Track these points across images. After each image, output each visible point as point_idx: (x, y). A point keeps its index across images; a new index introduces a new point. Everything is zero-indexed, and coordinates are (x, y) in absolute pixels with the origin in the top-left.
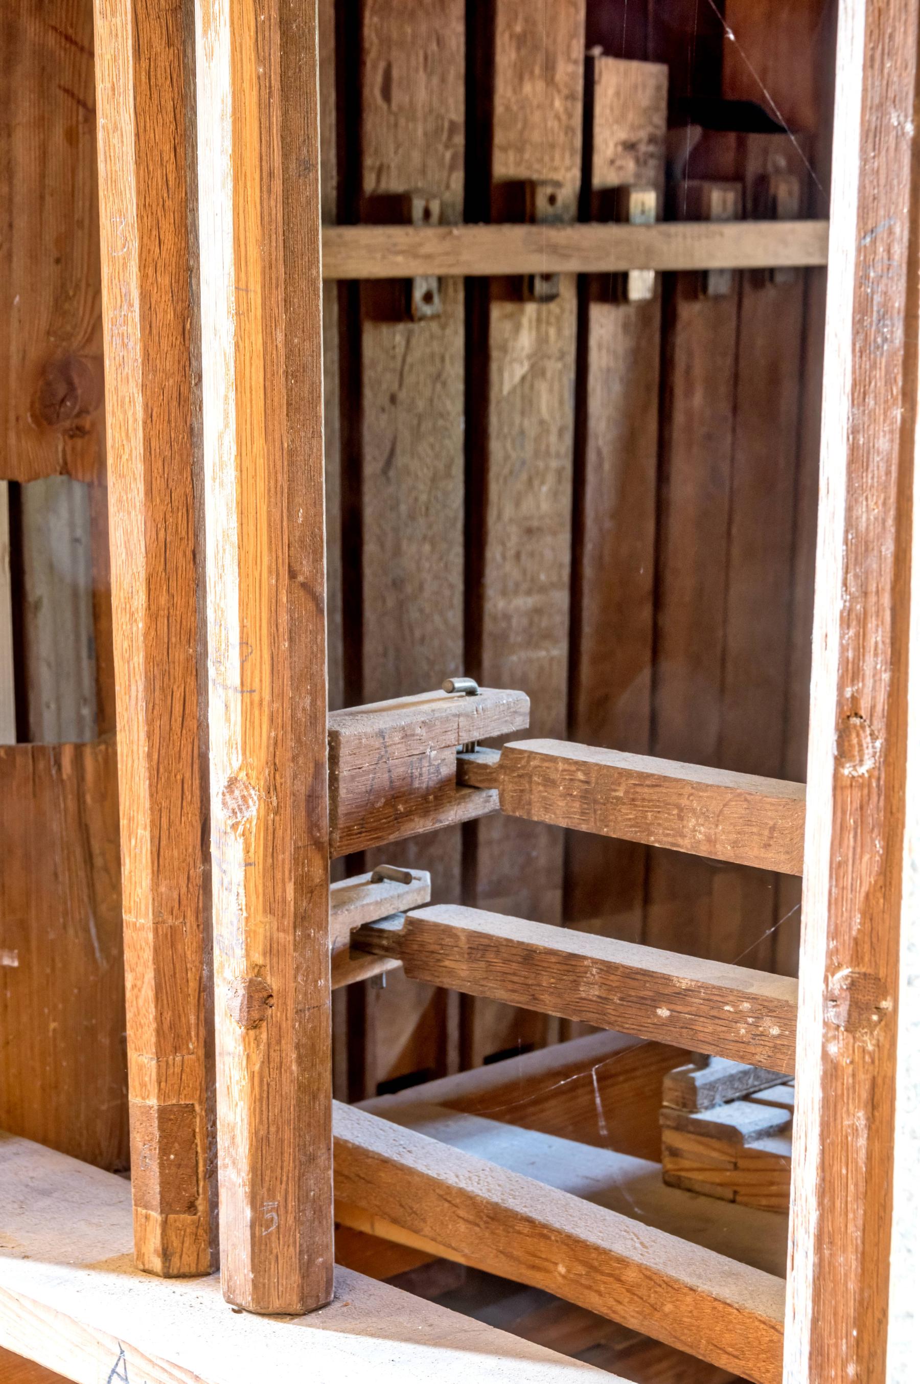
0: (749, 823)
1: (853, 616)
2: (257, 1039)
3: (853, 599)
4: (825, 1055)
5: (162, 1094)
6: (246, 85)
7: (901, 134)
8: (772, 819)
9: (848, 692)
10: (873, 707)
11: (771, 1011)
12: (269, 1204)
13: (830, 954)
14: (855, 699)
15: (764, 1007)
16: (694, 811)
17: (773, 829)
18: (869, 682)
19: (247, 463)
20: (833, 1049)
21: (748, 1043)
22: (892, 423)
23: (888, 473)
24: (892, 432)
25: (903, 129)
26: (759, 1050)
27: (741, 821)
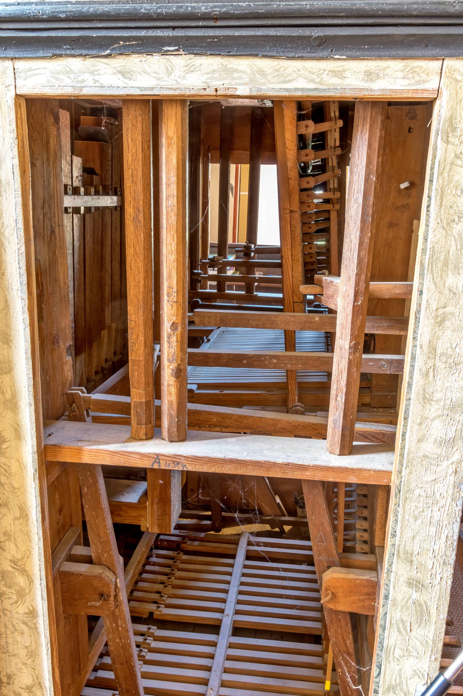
0: (267, 320)
2: (178, 380)
3: (359, 270)
4: (349, 358)
5: (146, 398)
6: (180, 161)
7: (373, 180)
9: (357, 289)
12: (181, 417)
13: (351, 339)
14: (358, 290)
16: (252, 320)
17: (274, 321)
19: (179, 249)
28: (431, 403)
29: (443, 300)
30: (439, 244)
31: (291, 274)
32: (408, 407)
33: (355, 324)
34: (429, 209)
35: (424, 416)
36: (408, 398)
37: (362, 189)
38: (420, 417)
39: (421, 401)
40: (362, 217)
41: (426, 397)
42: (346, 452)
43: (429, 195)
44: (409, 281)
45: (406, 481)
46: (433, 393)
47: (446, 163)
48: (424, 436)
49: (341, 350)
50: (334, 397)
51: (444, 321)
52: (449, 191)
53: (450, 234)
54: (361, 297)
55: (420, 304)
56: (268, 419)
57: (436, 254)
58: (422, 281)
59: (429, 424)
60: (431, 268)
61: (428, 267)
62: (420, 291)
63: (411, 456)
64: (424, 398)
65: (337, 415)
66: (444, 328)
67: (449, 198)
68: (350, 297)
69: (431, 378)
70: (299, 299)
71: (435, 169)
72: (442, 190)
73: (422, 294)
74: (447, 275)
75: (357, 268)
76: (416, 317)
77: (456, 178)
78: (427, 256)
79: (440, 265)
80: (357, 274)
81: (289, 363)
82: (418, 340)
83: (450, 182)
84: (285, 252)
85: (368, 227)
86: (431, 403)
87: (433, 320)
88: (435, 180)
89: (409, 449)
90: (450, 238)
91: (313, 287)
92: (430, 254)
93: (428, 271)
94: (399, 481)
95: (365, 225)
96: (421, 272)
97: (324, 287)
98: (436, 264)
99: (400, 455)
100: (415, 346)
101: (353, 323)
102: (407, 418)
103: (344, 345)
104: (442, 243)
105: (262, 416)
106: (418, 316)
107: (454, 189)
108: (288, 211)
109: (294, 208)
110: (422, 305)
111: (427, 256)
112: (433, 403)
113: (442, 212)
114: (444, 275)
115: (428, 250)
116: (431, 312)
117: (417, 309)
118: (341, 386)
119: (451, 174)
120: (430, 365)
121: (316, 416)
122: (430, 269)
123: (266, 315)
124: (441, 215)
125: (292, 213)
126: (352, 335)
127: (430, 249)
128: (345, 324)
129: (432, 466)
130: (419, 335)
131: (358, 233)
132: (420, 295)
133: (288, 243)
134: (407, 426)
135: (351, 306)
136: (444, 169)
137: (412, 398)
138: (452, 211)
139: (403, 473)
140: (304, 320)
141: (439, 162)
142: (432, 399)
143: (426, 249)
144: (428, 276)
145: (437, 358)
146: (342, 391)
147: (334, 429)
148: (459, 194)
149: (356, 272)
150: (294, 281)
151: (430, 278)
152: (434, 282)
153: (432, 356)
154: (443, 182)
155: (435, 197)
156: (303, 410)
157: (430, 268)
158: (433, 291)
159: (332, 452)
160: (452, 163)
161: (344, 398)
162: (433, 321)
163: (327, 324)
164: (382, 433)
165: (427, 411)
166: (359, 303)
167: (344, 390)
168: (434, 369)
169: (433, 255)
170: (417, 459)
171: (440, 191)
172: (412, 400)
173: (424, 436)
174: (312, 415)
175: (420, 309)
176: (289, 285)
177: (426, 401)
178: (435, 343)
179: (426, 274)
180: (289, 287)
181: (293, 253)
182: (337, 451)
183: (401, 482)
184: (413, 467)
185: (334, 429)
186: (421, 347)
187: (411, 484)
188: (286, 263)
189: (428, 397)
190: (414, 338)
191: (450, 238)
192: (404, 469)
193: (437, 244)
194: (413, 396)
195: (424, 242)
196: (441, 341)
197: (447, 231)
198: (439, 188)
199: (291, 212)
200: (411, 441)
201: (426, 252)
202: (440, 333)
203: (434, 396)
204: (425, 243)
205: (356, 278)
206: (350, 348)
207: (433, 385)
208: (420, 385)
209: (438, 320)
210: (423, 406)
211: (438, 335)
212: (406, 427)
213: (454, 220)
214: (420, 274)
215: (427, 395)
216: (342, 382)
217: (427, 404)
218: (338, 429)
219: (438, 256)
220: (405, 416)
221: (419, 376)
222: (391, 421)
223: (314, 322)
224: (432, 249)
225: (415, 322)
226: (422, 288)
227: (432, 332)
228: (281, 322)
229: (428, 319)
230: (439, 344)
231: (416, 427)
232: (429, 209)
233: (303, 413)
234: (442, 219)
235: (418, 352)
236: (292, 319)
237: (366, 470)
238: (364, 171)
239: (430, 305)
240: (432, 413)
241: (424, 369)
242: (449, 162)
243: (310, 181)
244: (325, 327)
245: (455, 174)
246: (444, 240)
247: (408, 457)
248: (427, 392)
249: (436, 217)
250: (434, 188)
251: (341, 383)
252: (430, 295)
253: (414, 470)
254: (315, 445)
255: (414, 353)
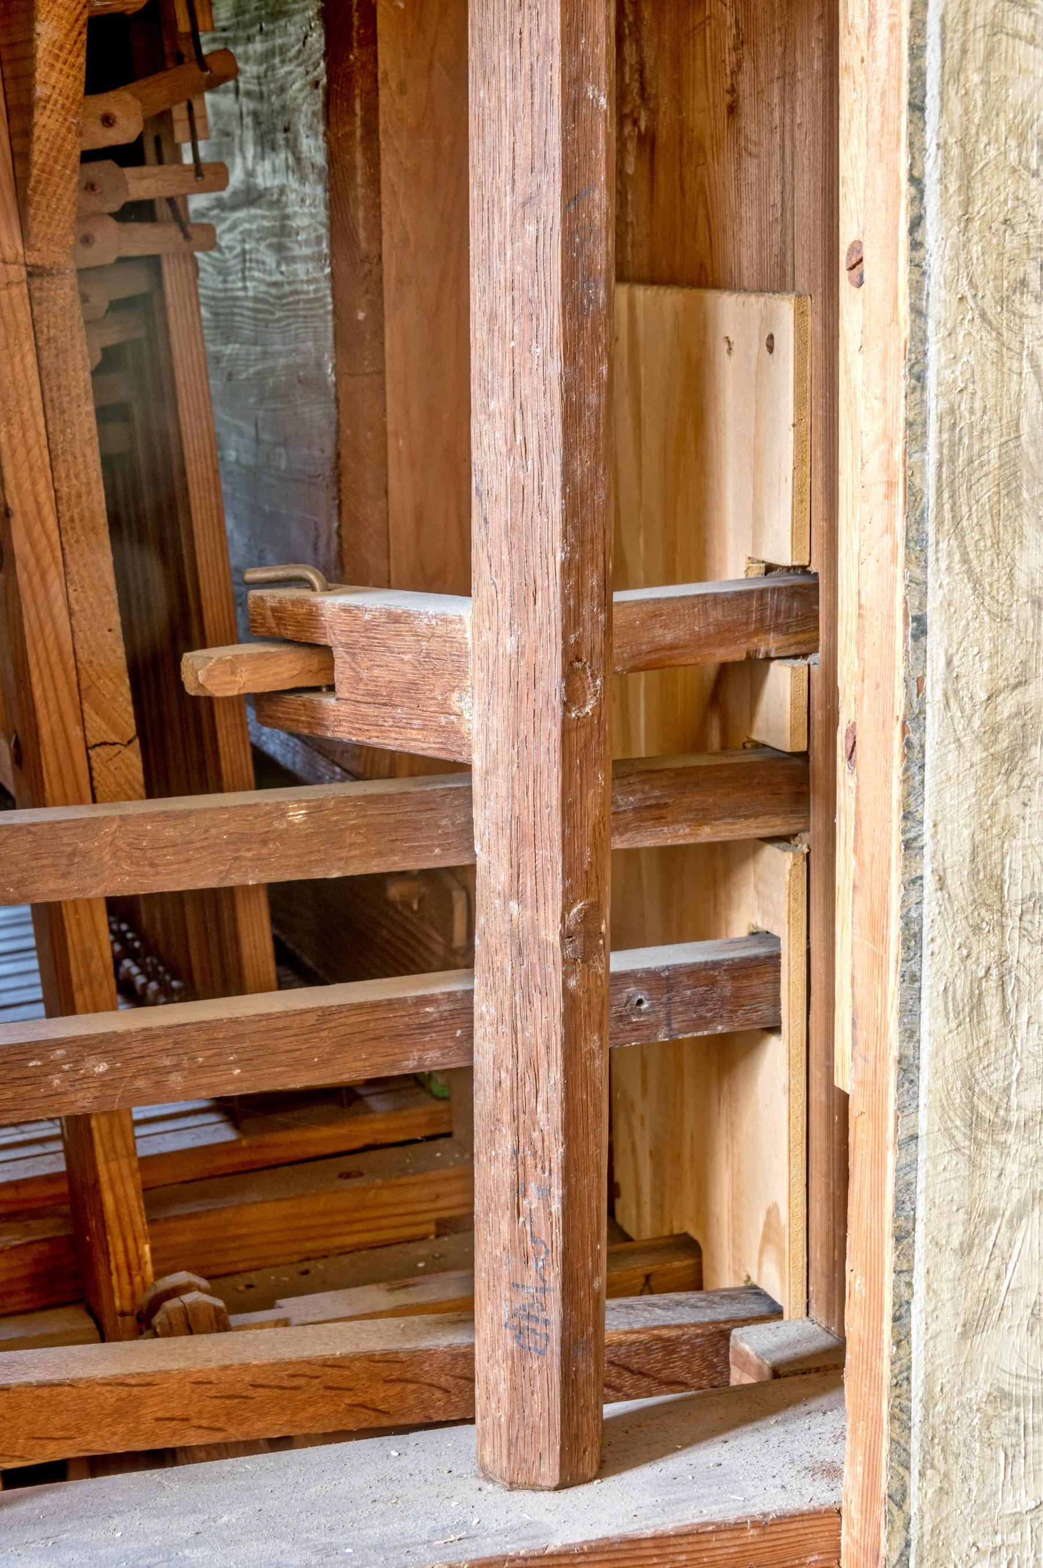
0: (36, 857)
1: (573, 566)
3: (573, 548)
4: (566, 992)
7: (595, 108)
8: (68, 845)
10: (593, 649)
11: (93, 1049)
13: (565, 894)
14: (577, 643)
15: (84, 1046)
18: (588, 625)
20: (572, 983)
21: (65, 1093)
22: (599, 379)
23: (597, 426)
24: (599, 387)
25: (598, 101)
26: (80, 1095)
27: (26, 856)
28: (1002, 1138)
29: (1014, 651)
30: (973, 394)
31: (60, 601)
32: (910, 1177)
33: (578, 817)
34: (918, 236)
35: (980, 1205)
36: (903, 1135)
37: (556, 153)
38: (962, 1216)
39: (959, 1137)
40: (566, 288)
41: (979, 1117)
42: (589, 1463)
43: (916, 174)
44: (636, 586)
45: (927, 1538)
46: (1007, 1089)
47: (971, 27)
48: (987, 1301)
49: (520, 953)
50: (506, 1195)
51: (1025, 749)
52: (992, 152)
53: (1015, 345)
54: (594, 679)
55: (920, 682)
56: (91, 1383)
57: (966, 441)
58: (917, 573)
59: (1003, 1242)
60: (952, 510)
61: (940, 505)
62: (916, 619)
63: (939, 1408)
64: (975, 1120)
65: (531, 1279)
66: (1027, 782)
67: (995, 183)
68: (542, 685)
69: (994, 1022)
70: (114, 728)
71: (929, 49)
72: (963, 146)
73: (924, 632)
74: (1018, 534)
75: (565, 536)
76: (908, 744)
77: (1016, 94)
78: (932, 456)
79: (986, 490)
80: (568, 568)
81: (177, 1067)
82: (927, 851)
83: (992, 111)
84: (18, 487)
85: (594, 330)
86: (1002, 1138)
87: (979, 748)
88: (932, 104)
89: (929, 1377)
90: (1015, 365)
91: (261, 656)
92: (941, 445)
93: (940, 522)
94: (898, 1542)
95: (581, 327)
96: (913, 533)
97: (339, 653)
98: (969, 489)
99: (893, 1417)
100: (913, 882)
101: (568, 809)
102: (908, 1233)
103: (535, 928)
104: (985, 390)
105: (56, 1377)
106: (914, 738)
107: (1013, 143)
108: (18, 273)
109: (46, 255)
110: (928, 683)
111: (932, 456)
112: (1010, 1137)
113: (976, 249)
114: (1007, 537)
115: (933, 426)
116: (968, 712)
117: (909, 705)
118: (536, 1135)
119: (994, 77)
120: (984, 963)
121: (286, 1323)
122: (948, 516)
123: (28, 829)
124: (968, 264)
125: (37, 282)
126: (568, 872)
127: (940, 419)
128: (528, 818)
129: (1030, 1439)
130: (927, 827)
131: (555, 367)
132: (916, 637)
133: (31, 436)
134: (910, 1271)
135: (552, 729)
136: (964, 52)
137: (922, 1131)
138: (1012, 243)
139: (913, 1505)
140: (232, 827)
141: (943, 20)
142: (1005, 1122)
143: (924, 423)
144: (943, 545)
145: (1012, 923)
146: (542, 1160)
147: (522, 1358)
148: (1034, 165)
149: (559, 556)
150: (80, 635)
151: (950, 555)
152: (970, 572)
153: (987, 916)
154: (966, 112)
155: (940, 180)
156: (220, 1303)
157: (947, 507)
158: (969, 614)
159: (521, 1479)
160: (993, 25)
161: (557, 1192)
162: (978, 754)
163: (351, 838)
164: (659, 1339)
165: (991, 1182)
166: (588, 709)
167: (557, 1153)
168: (1002, 977)
169: (952, 445)
170: (965, 1421)
171: (955, 151)
172: (922, 1141)
173: (987, 1301)
174: (262, 1326)
175: (922, 702)
176: (54, 657)
177: (981, 1136)
178: (996, 857)
179: (932, 539)
180: (58, 671)
181: (64, 490)
182: (549, 1469)
183: (908, 1545)
184: (951, 1459)
185: (522, 1358)
186: (942, 884)
187: (946, 1543)
188: (33, 545)
189: (988, 1114)
190: (907, 845)
191: (1015, 365)
192: (914, 1482)
193: (966, 396)
194: (924, 1121)
195: (914, 390)
196: (1019, 843)
197: (1000, 334)
198: (951, 140)
199: (30, 274)
200: (934, 1337)
201: (924, 434)
202: (1015, 804)
203: (1014, 1101)
204: (917, 395)
205: (563, 588)
206: (566, 936)
207: (1003, 1052)
208: (949, 1063)
209: (998, 747)
210: (972, 1162)
211: (1007, 816)
212: (905, 1278)
213: (1024, 283)
214: (908, 541)
215: (982, 1107)
216: (542, 1117)
217: (989, 1149)
218: (542, 1353)
219: (976, 448)
220: (901, 1222)
221: (941, 1021)
222: (648, 1277)
223: (282, 836)
224: (947, 421)
225: (906, 769)
226: (922, 605)
227: (979, 802)
228: (114, 855)
229: (960, 746)
230: (1015, 859)
231: (950, 1267)
232: (918, 236)
233: (219, 1324)
234: (980, 282)
235: (930, 910)
236: (169, 832)
237: (721, 1528)
238: (557, 64)
239: (963, 680)
240: (1011, 1188)
241: (961, 986)
242: (980, 20)
243: (116, 111)
244: (344, 853)
245: (1011, 74)
246: (991, 375)
247: (926, 1418)
248: (983, 1092)
249: (949, 270)
250: (931, 139)
251: (535, 1123)
252: (957, 635)
253: (956, 1477)
254: (404, 1461)
255: (914, 914)
